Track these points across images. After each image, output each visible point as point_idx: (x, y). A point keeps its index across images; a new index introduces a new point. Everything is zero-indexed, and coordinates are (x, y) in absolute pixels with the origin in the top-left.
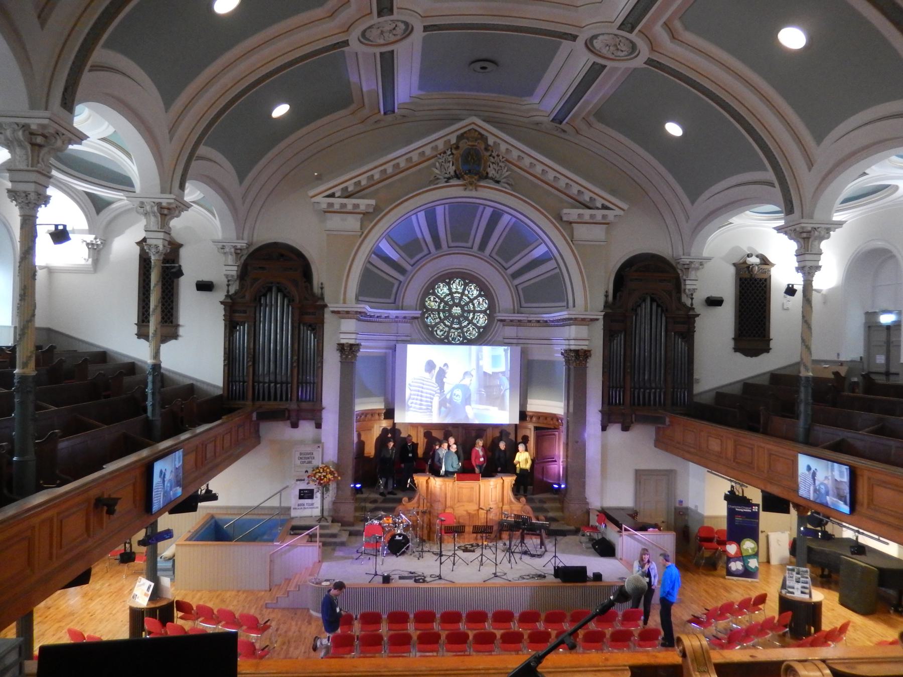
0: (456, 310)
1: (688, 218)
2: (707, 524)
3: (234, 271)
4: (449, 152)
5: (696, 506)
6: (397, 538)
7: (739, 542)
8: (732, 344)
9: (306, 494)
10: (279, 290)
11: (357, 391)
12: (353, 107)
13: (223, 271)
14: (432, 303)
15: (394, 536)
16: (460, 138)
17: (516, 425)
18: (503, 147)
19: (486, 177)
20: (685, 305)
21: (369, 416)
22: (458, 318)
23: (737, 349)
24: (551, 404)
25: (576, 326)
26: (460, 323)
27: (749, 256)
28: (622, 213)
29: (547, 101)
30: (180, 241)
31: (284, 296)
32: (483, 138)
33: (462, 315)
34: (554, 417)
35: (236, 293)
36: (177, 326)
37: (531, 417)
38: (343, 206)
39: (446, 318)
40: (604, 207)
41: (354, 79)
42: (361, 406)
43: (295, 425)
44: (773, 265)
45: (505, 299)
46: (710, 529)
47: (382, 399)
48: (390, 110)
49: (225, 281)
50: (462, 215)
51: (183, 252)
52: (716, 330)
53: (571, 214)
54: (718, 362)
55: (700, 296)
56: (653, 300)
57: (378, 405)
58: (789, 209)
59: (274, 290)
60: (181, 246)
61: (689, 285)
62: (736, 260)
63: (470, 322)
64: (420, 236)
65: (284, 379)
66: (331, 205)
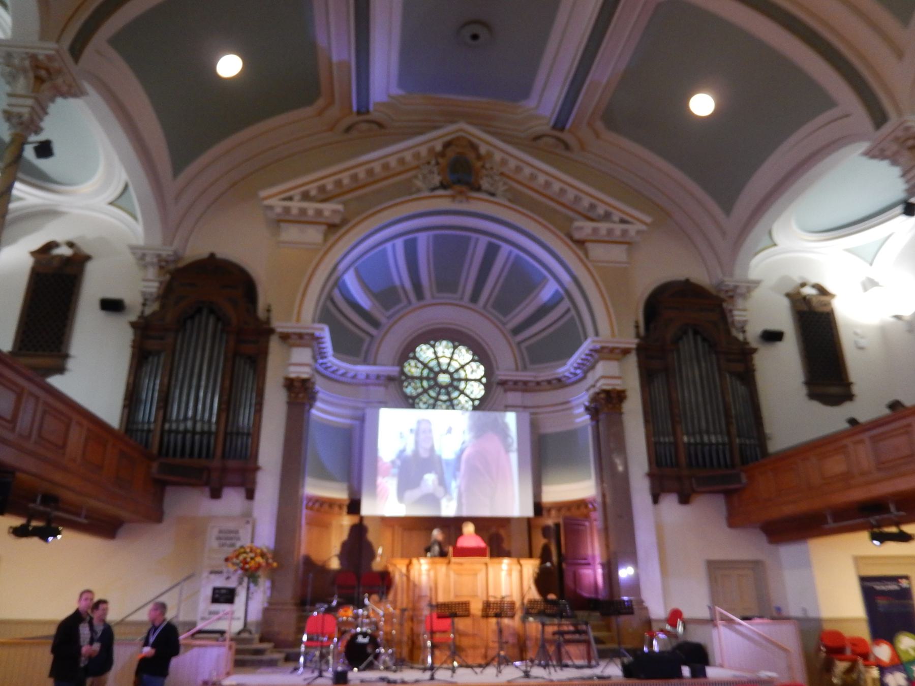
0: (444, 379)
1: (724, 233)
2: (828, 627)
3: (153, 287)
4: (433, 162)
5: (804, 610)
6: (361, 640)
7: (890, 640)
8: (803, 391)
9: (224, 596)
10: (212, 311)
11: (309, 466)
12: (321, 102)
13: (138, 287)
14: (412, 369)
15: (355, 636)
16: (447, 145)
17: (529, 520)
18: (498, 156)
19: (479, 189)
20: (736, 339)
21: (326, 507)
22: (446, 387)
23: (812, 396)
24: (575, 487)
25: (603, 358)
26: (448, 394)
27: (803, 285)
28: (643, 227)
29: (546, 100)
30: (87, 250)
31: (218, 319)
32: (474, 147)
33: (451, 385)
34: (582, 504)
35: (154, 314)
36: (66, 356)
37: (549, 510)
38: (303, 211)
39: (430, 387)
40: (623, 221)
41: (321, 41)
42: (313, 488)
43: (216, 494)
44: (833, 296)
45: (507, 369)
46: (838, 635)
47: (345, 486)
48: (364, 109)
49: (140, 300)
50: (450, 249)
51: (90, 267)
52: (781, 372)
53: (584, 228)
54: (789, 411)
55: (753, 332)
56: (696, 333)
57: (338, 493)
58: (879, 118)
59: (205, 312)
60: (88, 258)
61: (738, 316)
62: (789, 289)
63: (462, 392)
64: (397, 283)
65: (206, 428)
66: (287, 210)
